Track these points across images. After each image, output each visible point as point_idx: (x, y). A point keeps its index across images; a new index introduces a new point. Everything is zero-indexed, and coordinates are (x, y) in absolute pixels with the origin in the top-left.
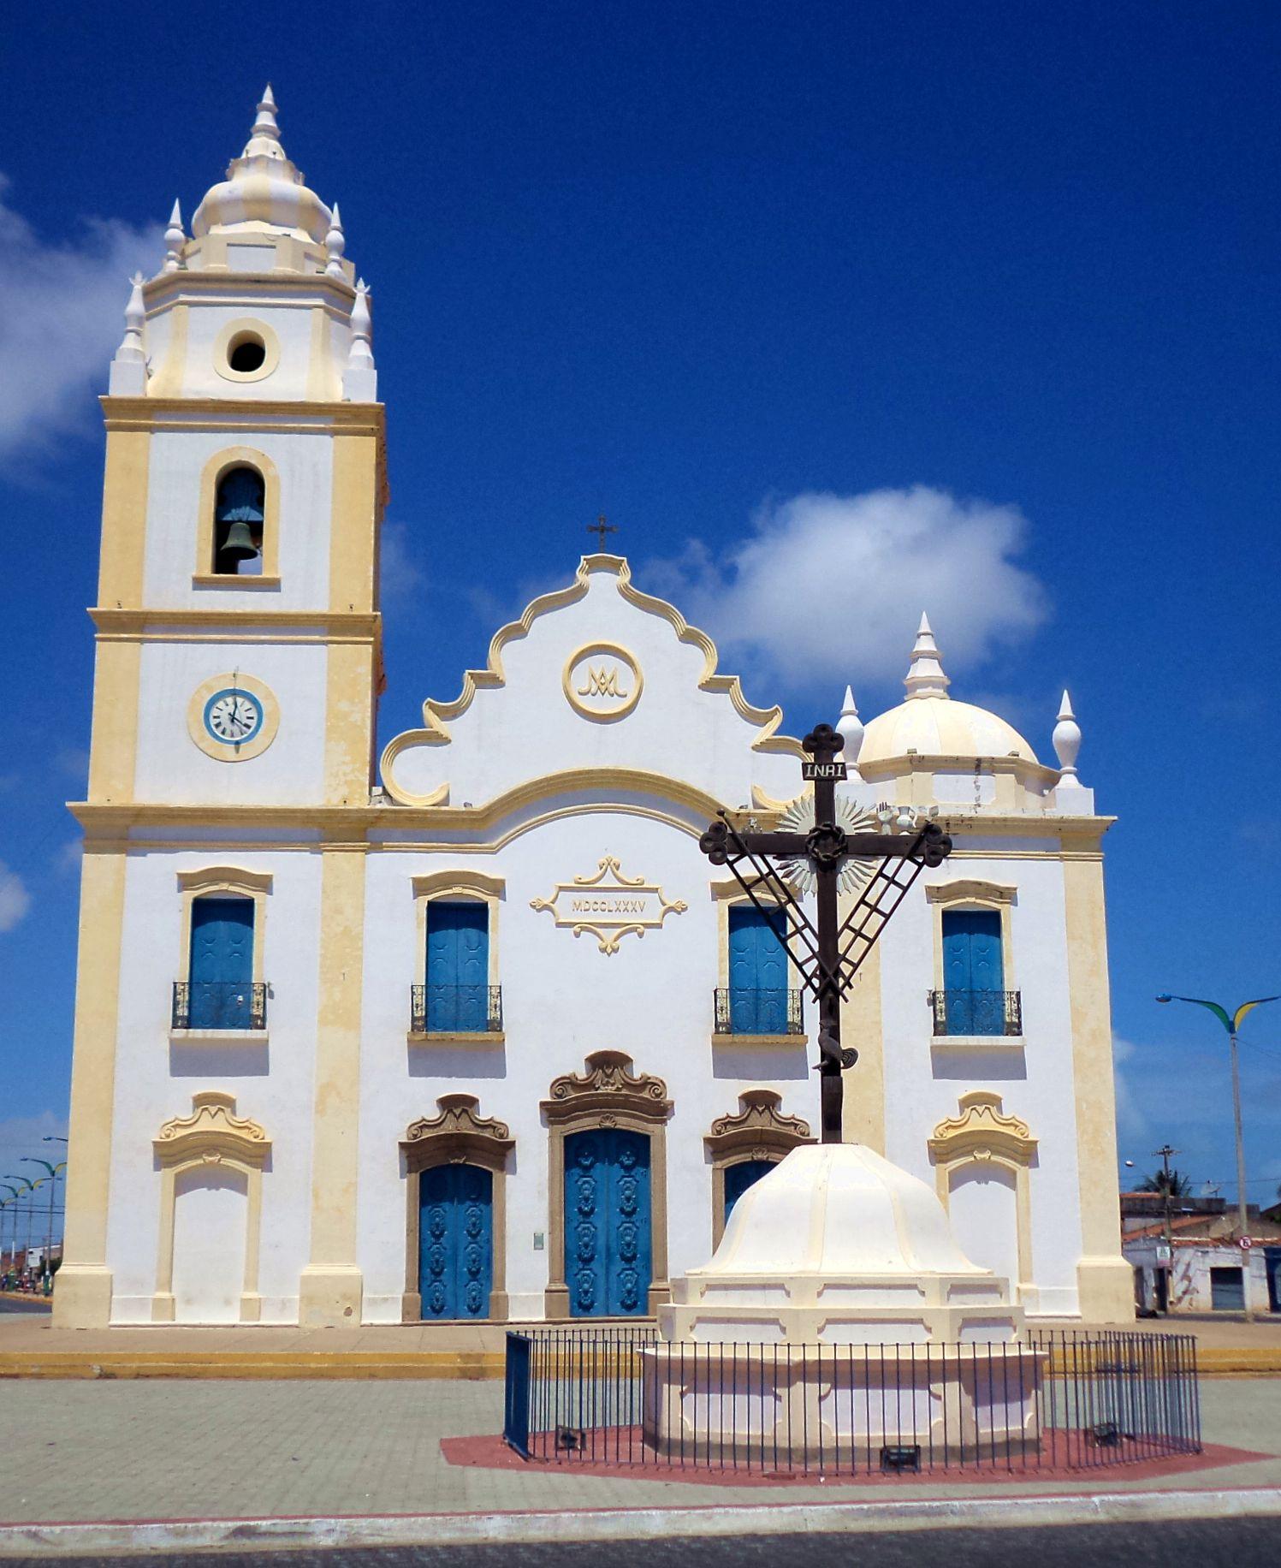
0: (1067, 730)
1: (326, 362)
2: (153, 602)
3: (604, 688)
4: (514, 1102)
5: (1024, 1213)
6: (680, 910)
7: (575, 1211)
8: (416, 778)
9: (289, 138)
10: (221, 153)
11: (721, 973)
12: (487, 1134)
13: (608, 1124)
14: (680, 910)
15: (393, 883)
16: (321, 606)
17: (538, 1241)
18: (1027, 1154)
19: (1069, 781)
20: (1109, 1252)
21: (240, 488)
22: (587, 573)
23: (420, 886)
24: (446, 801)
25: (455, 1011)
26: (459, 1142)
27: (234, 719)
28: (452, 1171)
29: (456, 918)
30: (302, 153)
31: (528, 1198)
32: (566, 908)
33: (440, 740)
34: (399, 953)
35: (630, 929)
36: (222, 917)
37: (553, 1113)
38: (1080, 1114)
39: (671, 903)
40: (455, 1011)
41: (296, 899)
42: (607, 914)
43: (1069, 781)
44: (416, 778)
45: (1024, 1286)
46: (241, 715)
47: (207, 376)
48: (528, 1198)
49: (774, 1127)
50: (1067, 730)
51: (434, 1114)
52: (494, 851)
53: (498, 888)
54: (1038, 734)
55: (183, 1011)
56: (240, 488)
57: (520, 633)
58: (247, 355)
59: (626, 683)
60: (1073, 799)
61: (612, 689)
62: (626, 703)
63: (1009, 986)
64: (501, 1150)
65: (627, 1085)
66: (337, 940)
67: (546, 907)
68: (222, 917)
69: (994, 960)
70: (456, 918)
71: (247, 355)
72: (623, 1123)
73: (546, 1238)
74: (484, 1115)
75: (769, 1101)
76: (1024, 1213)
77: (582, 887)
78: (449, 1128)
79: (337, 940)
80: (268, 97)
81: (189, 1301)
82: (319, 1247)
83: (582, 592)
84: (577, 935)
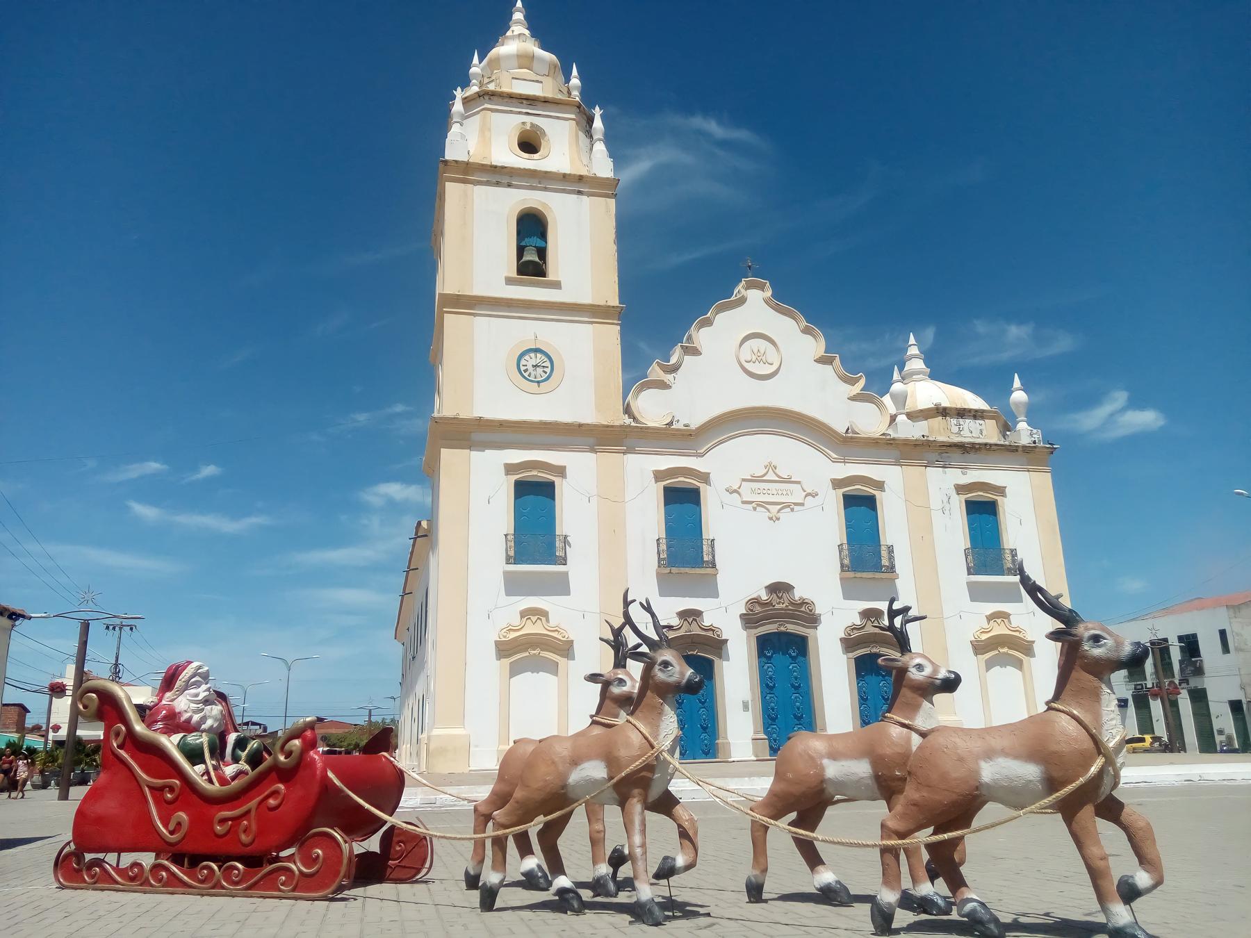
3: (760, 358)
15: (641, 474)
17: (746, 706)
23: (659, 476)
30: (538, 30)
39: (809, 491)
42: (772, 499)
44: (652, 408)
52: (702, 455)
53: (705, 478)
57: (709, 323)
60: (1024, 433)
66: (607, 509)
67: (735, 491)
72: (791, 628)
77: (754, 479)
79: (607, 509)
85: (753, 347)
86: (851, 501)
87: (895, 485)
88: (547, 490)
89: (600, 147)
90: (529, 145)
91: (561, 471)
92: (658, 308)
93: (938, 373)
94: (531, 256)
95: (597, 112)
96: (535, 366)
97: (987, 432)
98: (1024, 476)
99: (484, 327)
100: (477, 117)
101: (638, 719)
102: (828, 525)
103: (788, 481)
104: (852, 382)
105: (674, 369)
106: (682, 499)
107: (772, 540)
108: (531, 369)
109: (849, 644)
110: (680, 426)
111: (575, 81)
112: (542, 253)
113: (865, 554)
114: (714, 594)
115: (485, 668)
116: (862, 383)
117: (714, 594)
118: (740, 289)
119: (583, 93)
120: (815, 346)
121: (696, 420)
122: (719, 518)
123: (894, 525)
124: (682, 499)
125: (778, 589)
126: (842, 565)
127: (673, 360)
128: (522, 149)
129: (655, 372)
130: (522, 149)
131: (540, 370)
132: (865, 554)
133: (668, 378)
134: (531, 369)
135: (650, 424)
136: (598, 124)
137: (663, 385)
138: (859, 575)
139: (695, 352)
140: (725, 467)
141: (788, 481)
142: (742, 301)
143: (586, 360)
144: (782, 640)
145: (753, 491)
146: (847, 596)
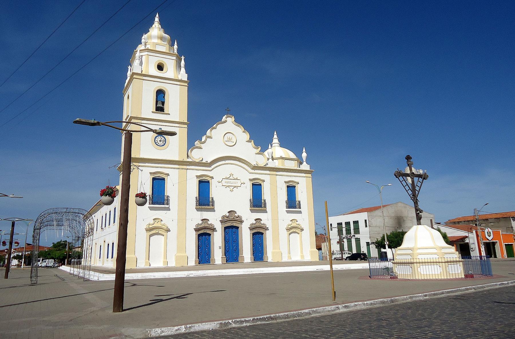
0: (304, 155)
1: (176, 72)
3: (229, 140)
4: (215, 218)
5: (301, 237)
8: (196, 155)
9: (161, 22)
10: (151, 23)
12: (210, 226)
15: (192, 177)
17: (220, 248)
19: (305, 163)
21: (160, 93)
23: (197, 177)
25: (204, 201)
28: (204, 236)
30: (164, 25)
31: (218, 240)
34: (193, 191)
40: (204, 201)
42: (231, 183)
43: (305, 163)
44: (196, 155)
47: (154, 71)
48: (218, 240)
50: (304, 155)
51: (201, 222)
53: (212, 178)
54: (298, 154)
56: (160, 93)
57: (215, 128)
58: (160, 67)
60: (305, 166)
63: (210, 196)
66: (181, 187)
76: (301, 237)
80: (157, 16)
85: (228, 136)
86: (200, 182)
87: (266, 178)
89: (183, 70)
90: (160, 67)
92: (198, 126)
93: (282, 145)
94: (160, 105)
95: (183, 58)
96: (160, 141)
97: (293, 165)
99: (136, 257)
102: (247, 193)
103: (237, 179)
104: (258, 148)
105: (204, 142)
106: (204, 185)
107: (231, 199)
108: (159, 142)
109: (251, 229)
110: (204, 161)
111: (176, 46)
112: (163, 103)
113: (257, 203)
114: (213, 210)
115: (283, 233)
116: (260, 148)
117: (213, 210)
118: (224, 118)
119: (178, 50)
120: (247, 136)
122: (216, 192)
124: (204, 185)
127: (203, 140)
128: (156, 68)
129: (197, 143)
130: (156, 68)
131: (162, 142)
132: (257, 203)
133: (202, 145)
134: (159, 142)
136: (183, 62)
137: (201, 148)
138: (255, 208)
139: (210, 137)
140: (217, 175)
141: (237, 179)
142: (225, 122)
143: (175, 148)
144: (231, 230)
145: (226, 182)
146: (252, 211)
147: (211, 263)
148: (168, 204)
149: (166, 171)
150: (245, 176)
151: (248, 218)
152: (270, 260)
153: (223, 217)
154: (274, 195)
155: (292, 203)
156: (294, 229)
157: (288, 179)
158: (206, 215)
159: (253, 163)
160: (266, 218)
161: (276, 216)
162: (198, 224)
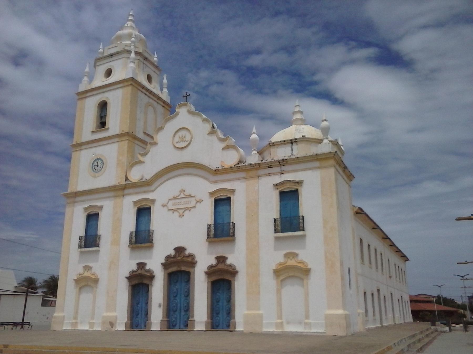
2: (84, 140)
4: (155, 262)
6: (201, 201)
7: (170, 295)
11: (211, 220)
12: (301, 265)
13: (179, 269)
14: (164, 206)
16: (117, 132)
17: (160, 306)
18: (307, 271)
20: (338, 308)
22: (179, 109)
23: (276, 185)
24: (141, 179)
25: (142, 238)
26: (141, 276)
27: (97, 165)
29: (143, 212)
32: (170, 206)
33: (142, 162)
35: (186, 209)
36: (92, 218)
37: (165, 266)
38: (326, 257)
39: (198, 200)
40: (142, 238)
41: (240, 191)
45: (306, 321)
46: (99, 164)
49: (225, 268)
52: (153, 191)
55: (134, 240)
59: (188, 138)
61: (184, 140)
62: (188, 143)
63: (300, 214)
64: (152, 277)
65: (184, 256)
66: (118, 220)
67: (165, 205)
68: (92, 218)
69: (297, 206)
70: (143, 212)
71: (109, 73)
72: (183, 268)
73: (162, 305)
74: (147, 267)
75: (295, 255)
77: (176, 198)
78: (139, 272)
79: (118, 220)
81: (81, 323)
82: (106, 307)
83: (178, 114)
84: (173, 212)
86: (282, 194)
87: (240, 191)
88: (295, 193)
91: (299, 183)
98: (309, 173)
100: (121, 60)
101: (339, 316)
107: (182, 228)
113: (221, 231)
115: (268, 281)
121: (148, 176)
122: (159, 221)
123: (238, 214)
125: (180, 250)
126: (131, 241)
132: (221, 231)
135: (133, 181)
140: (160, 195)
147: (232, 329)
148: (98, 247)
149: (98, 204)
150: (202, 189)
151: (204, 259)
152: (239, 328)
153: (168, 257)
154: (116, 228)
155: (290, 222)
156: (294, 272)
157: (278, 179)
158: (141, 257)
159: (214, 167)
160: (237, 257)
161: (255, 250)
162: (133, 272)
